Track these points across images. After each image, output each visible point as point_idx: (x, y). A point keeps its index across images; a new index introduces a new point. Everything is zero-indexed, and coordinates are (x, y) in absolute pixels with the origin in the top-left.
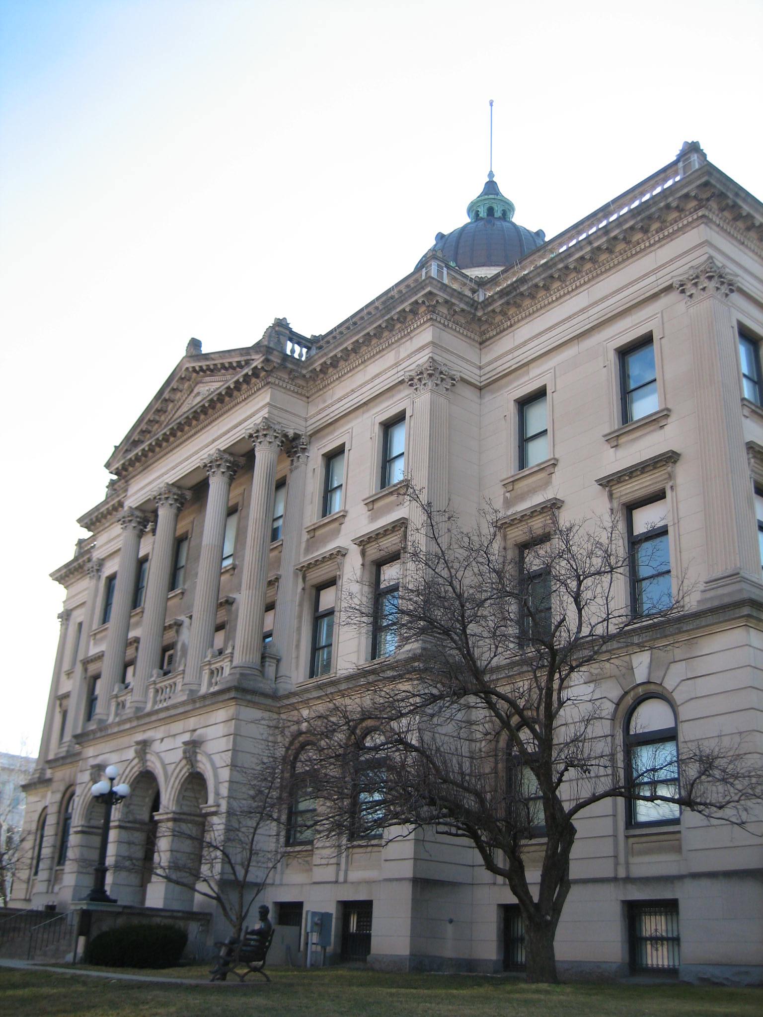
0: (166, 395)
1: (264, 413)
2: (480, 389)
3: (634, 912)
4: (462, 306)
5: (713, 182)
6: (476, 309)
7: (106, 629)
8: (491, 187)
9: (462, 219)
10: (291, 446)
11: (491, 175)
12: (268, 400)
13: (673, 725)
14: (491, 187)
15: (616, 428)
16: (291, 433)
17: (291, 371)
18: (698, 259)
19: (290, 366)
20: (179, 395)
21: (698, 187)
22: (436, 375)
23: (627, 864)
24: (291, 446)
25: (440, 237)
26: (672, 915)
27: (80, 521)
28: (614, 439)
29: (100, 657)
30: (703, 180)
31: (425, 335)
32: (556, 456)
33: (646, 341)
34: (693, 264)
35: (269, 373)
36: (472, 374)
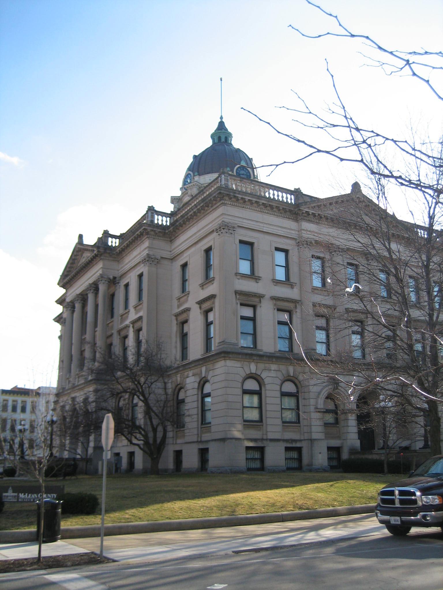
0: (73, 257)
1: (100, 272)
2: (172, 259)
4: (159, 230)
5: (222, 192)
6: (165, 230)
7: (112, 321)
8: (221, 125)
9: (209, 143)
10: (113, 282)
11: (221, 118)
12: (101, 266)
14: (221, 125)
16: (111, 277)
17: (109, 253)
18: (219, 221)
19: (108, 251)
20: (78, 257)
21: (218, 194)
22: (149, 259)
23: (201, 437)
24: (113, 282)
25: (195, 157)
27: (56, 302)
29: (140, 318)
30: (219, 192)
31: (146, 244)
35: (101, 255)
36: (166, 254)
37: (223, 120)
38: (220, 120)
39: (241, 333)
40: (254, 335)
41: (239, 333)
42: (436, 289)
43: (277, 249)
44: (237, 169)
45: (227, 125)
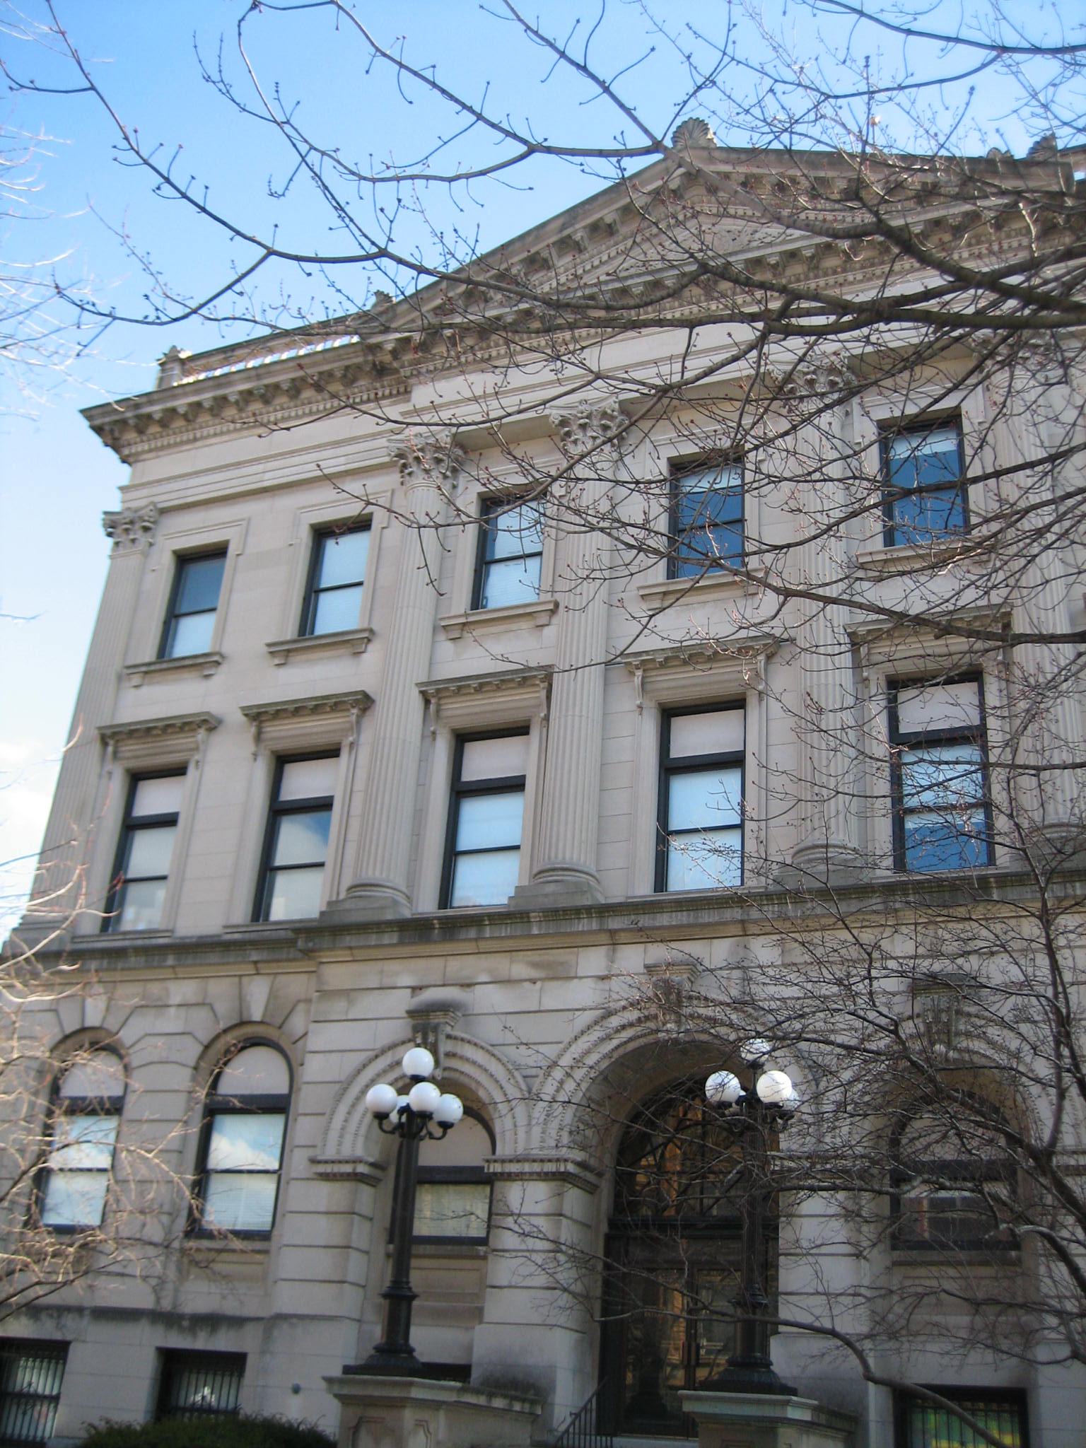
3: (173, 1367)
13: (285, 1090)
15: (288, 638)
26: (231, 1376)
28: (282, 653)
32: (374, 627)
33: (218, 552)
34: (156, 499)
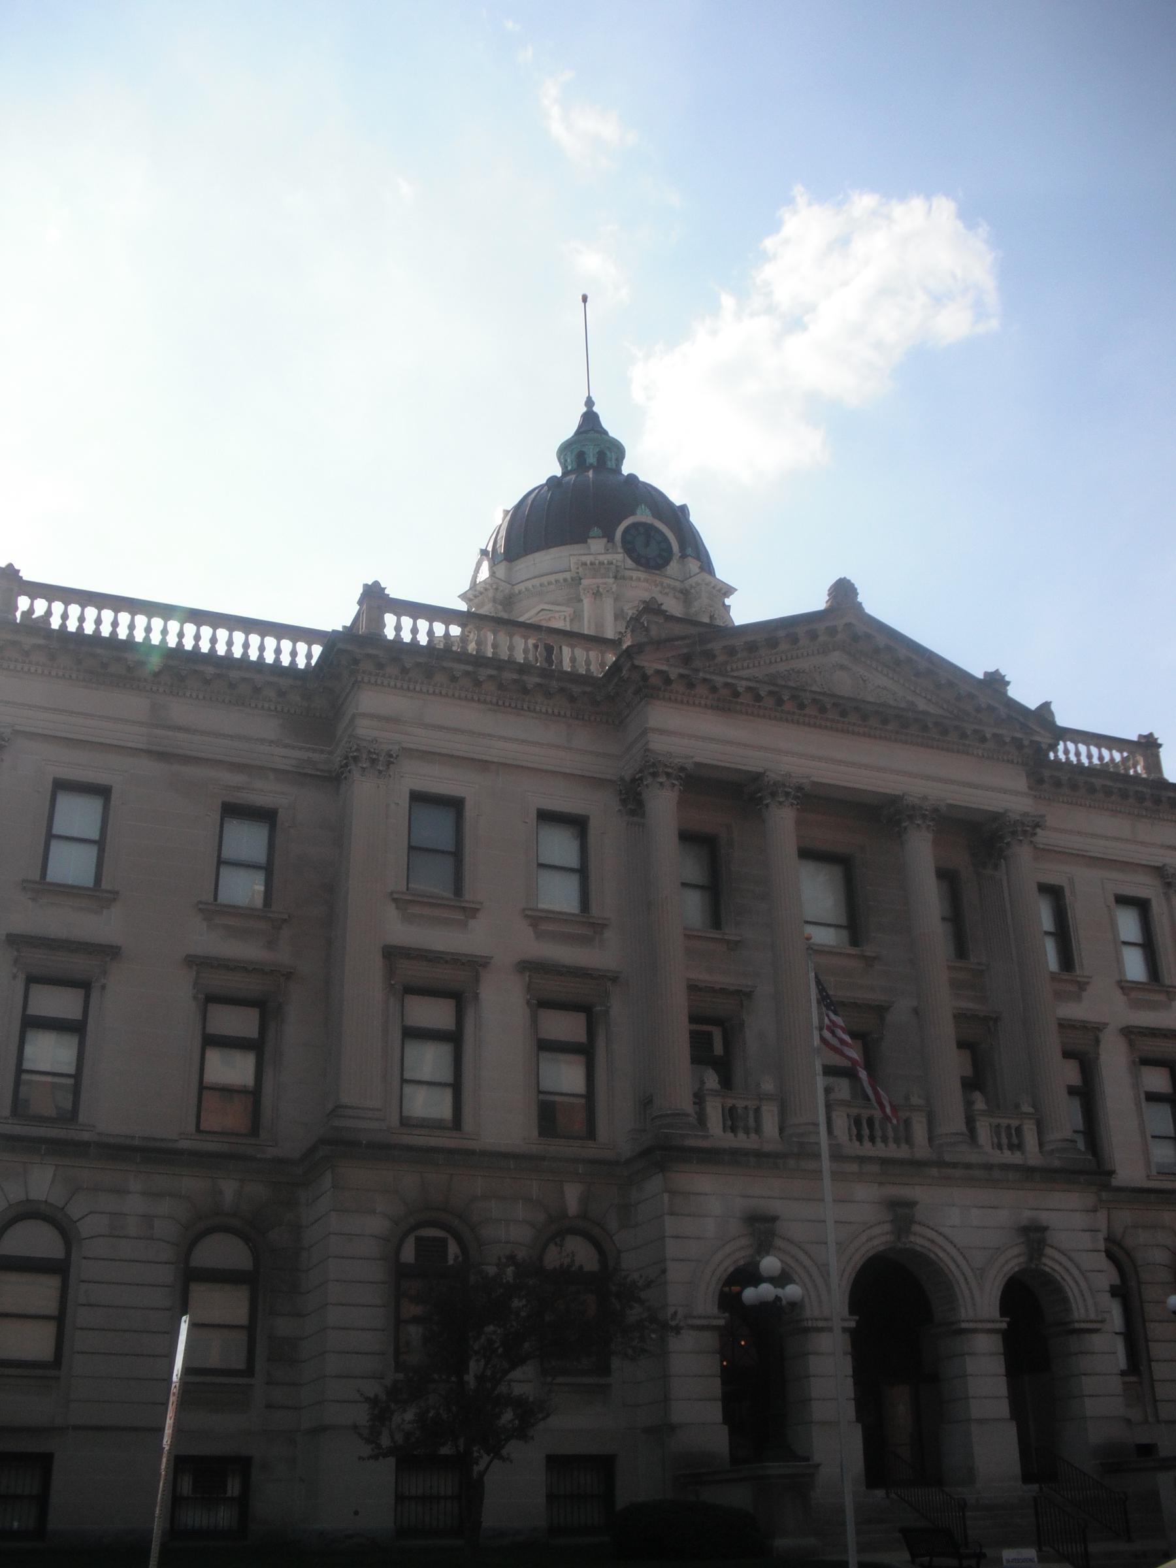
8: (590, 420)
11: (589, 402)
14: (590, 420)
37: (595, 409)
38: (584, 409)
39: (1153, 1137)
40: (457, 1087)
41: (1149, 1138)
42: (1117, 756)
43: (1122, 900)
44: (626, 531)
45: (606, 423)
